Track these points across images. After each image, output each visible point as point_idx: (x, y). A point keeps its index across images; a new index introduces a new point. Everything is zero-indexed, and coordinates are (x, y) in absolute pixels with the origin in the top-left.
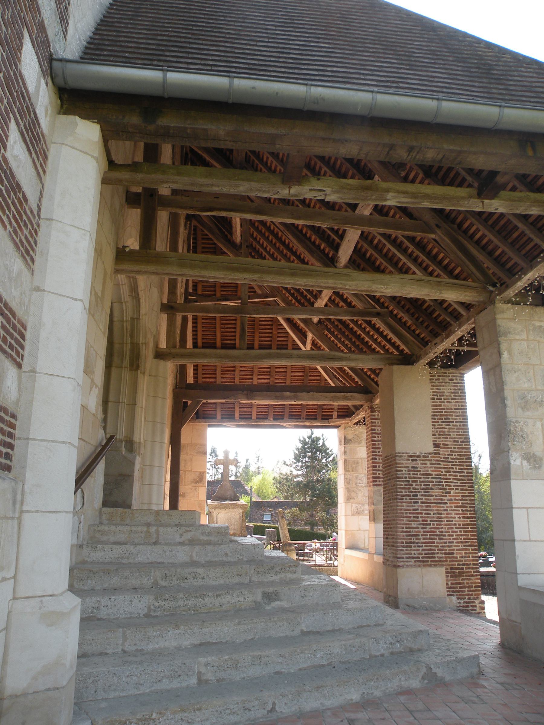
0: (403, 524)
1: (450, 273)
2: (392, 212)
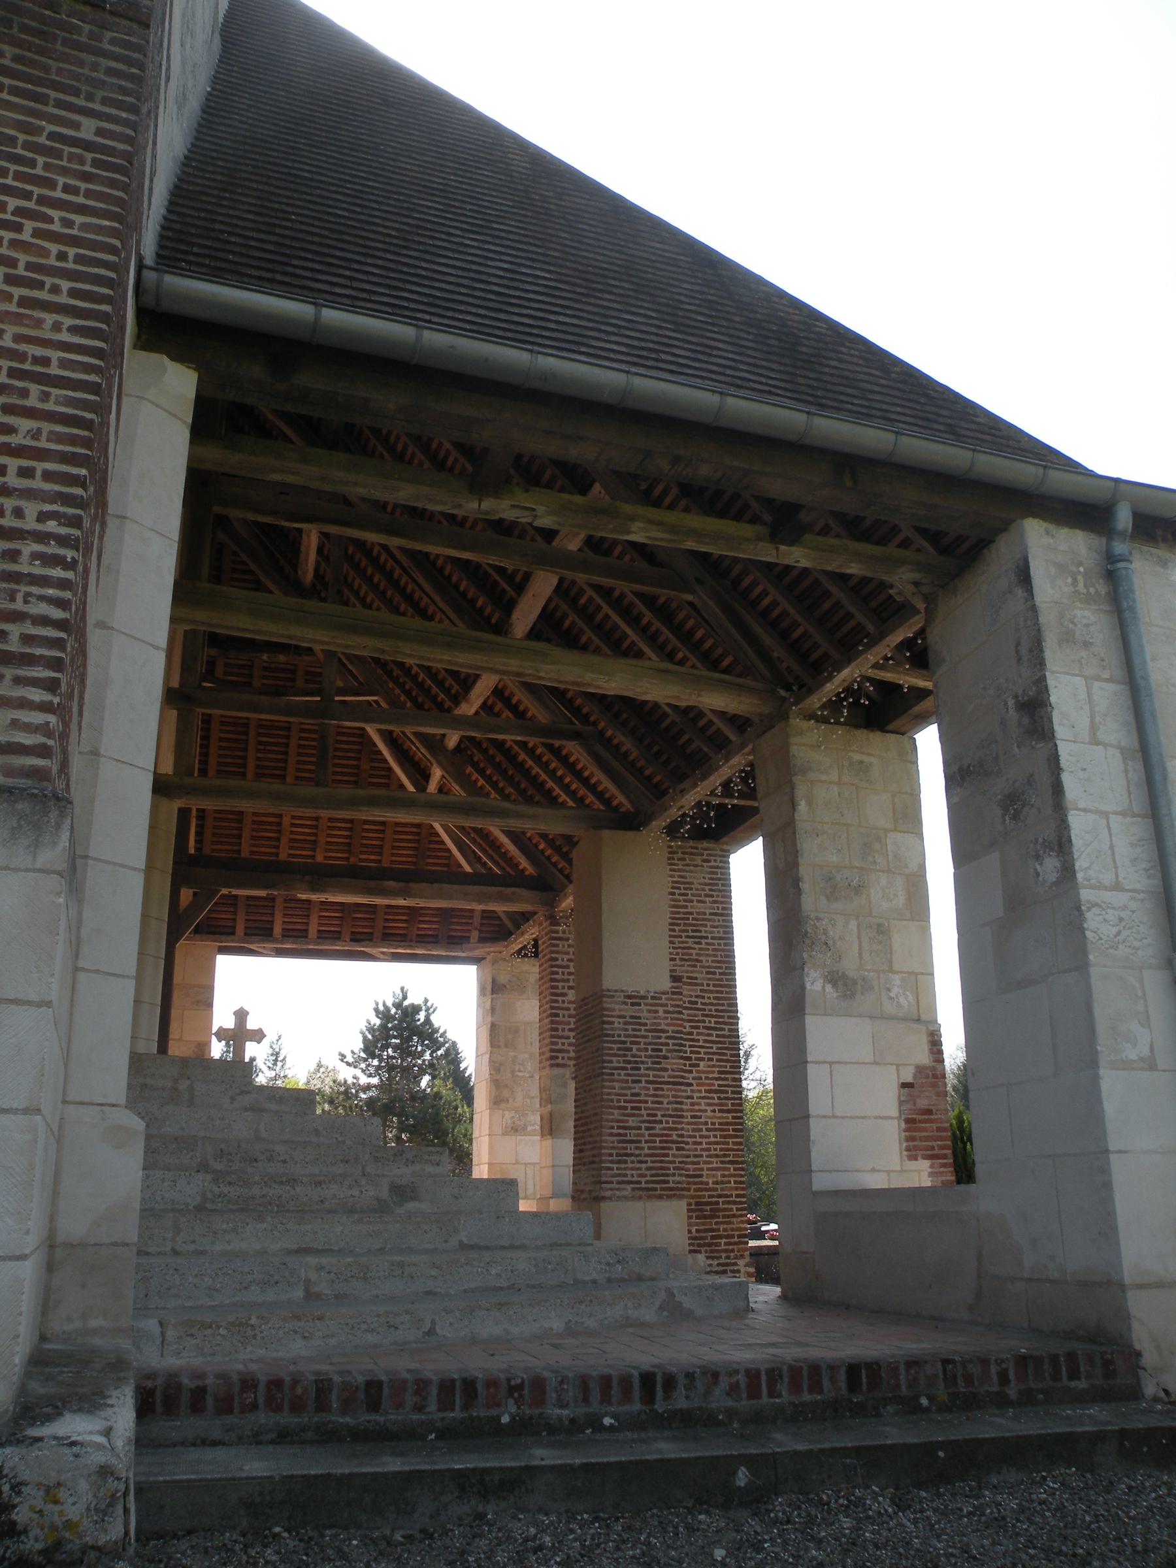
0: (613, 1120)
1: (714, 665)
2: (619, 548)
